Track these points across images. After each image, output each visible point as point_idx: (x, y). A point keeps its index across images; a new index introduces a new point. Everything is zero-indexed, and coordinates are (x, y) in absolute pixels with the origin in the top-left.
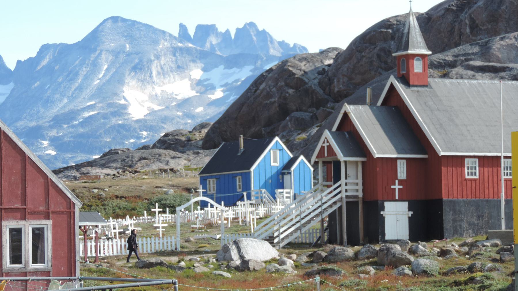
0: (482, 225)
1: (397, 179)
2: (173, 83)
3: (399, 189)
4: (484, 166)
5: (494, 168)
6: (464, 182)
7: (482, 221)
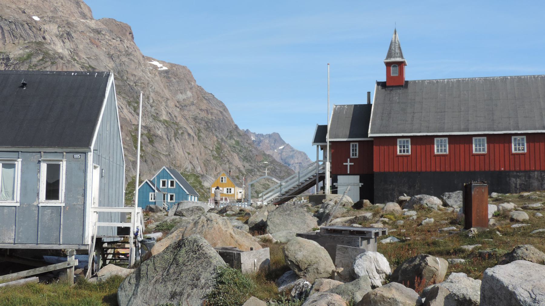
1: (349, 157)
2: (200, 87)
3: (350, 165)
6: (472, 158)
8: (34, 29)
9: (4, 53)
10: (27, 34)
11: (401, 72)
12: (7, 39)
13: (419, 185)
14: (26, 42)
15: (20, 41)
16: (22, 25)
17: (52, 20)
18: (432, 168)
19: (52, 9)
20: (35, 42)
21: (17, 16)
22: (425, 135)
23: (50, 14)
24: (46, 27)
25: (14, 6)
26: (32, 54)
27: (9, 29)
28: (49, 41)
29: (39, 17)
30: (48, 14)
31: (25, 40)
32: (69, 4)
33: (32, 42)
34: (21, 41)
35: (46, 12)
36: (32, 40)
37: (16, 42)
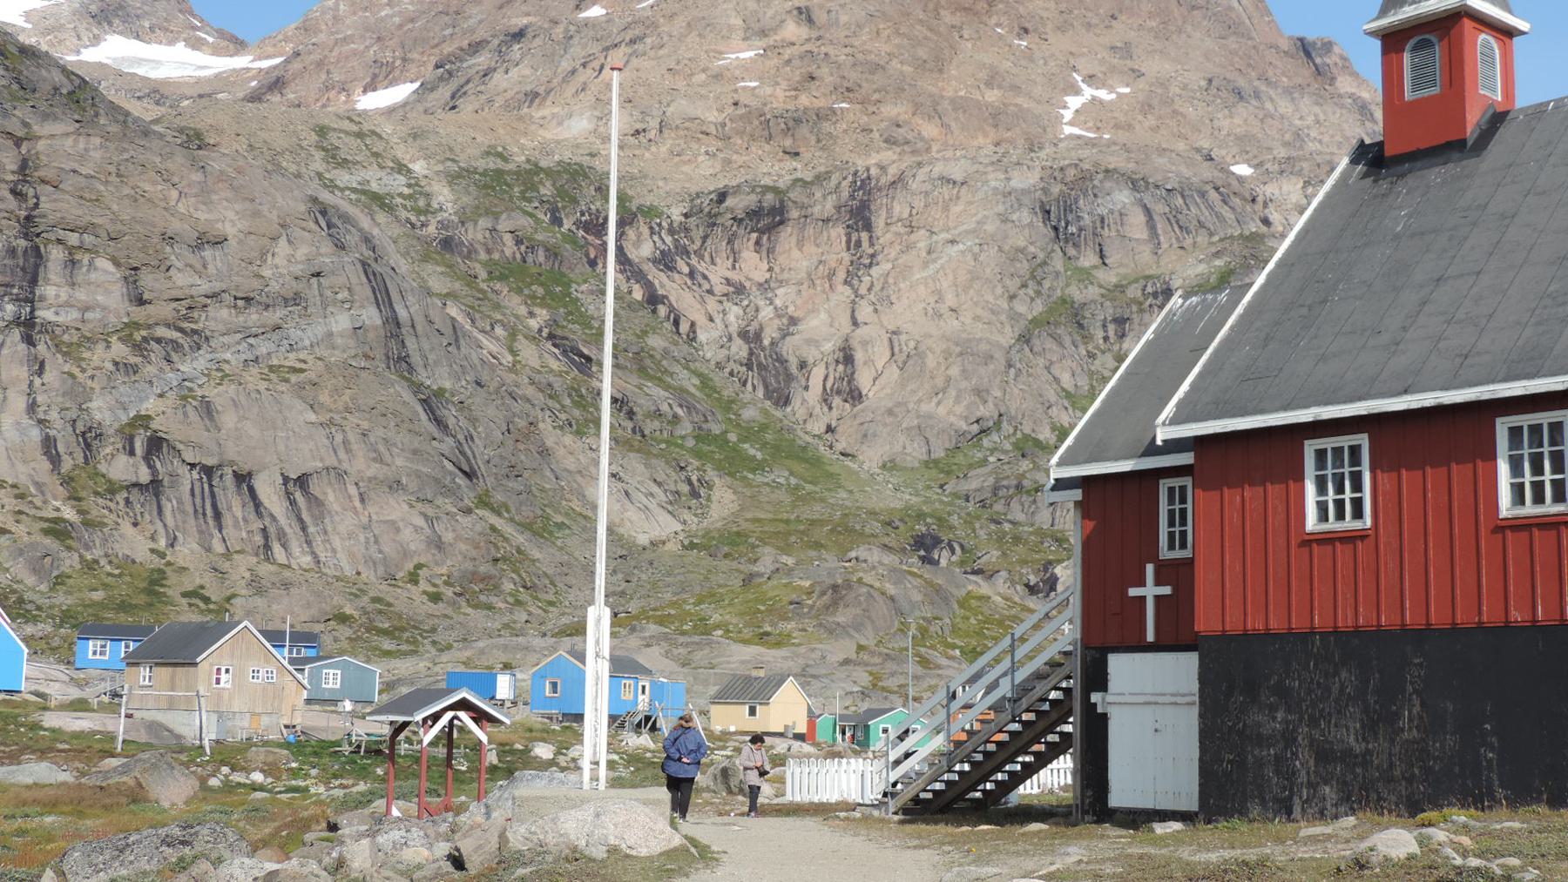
0: (1391, 766)
1: (1154, 557)
3: (1158, 598)
4: (1395, 467)
5: (1269, 486)
7: (1392, 741)
8: (1237, 201)
9: (1158, 277)
10: (1217, 217)
11: (1455, 74)
12: (1162, 238)
13: (1417, 709)
14: (1216, 238)
15: (1199, 239)
16: (1203, 194)
17: (1287, 167)
18: (1228, 619)
19: (1288, 137)
20: (1241, 235)
21: (1186, 172)
22: (1427, 403)
23: (1282, 153)
24: (1270, 190)
25: (1181, 146)
26: (1231, 272)
27: (1167, 210)
28: (1280, 229)
29: (1250, 166)
30: (1275, 152)
31: (1211, 234)
32: (1338, 115)
33: (1232, 237)
34: (1202, 239)
35: (1270, 149)
36: (1229, 231)
37: (1188, 241)
